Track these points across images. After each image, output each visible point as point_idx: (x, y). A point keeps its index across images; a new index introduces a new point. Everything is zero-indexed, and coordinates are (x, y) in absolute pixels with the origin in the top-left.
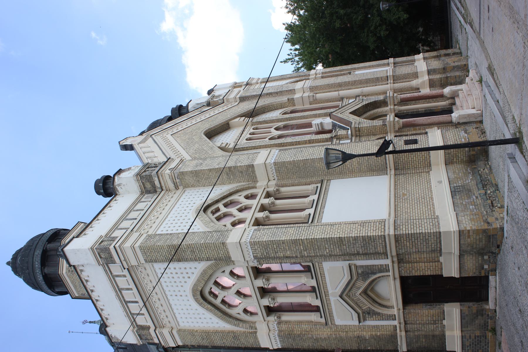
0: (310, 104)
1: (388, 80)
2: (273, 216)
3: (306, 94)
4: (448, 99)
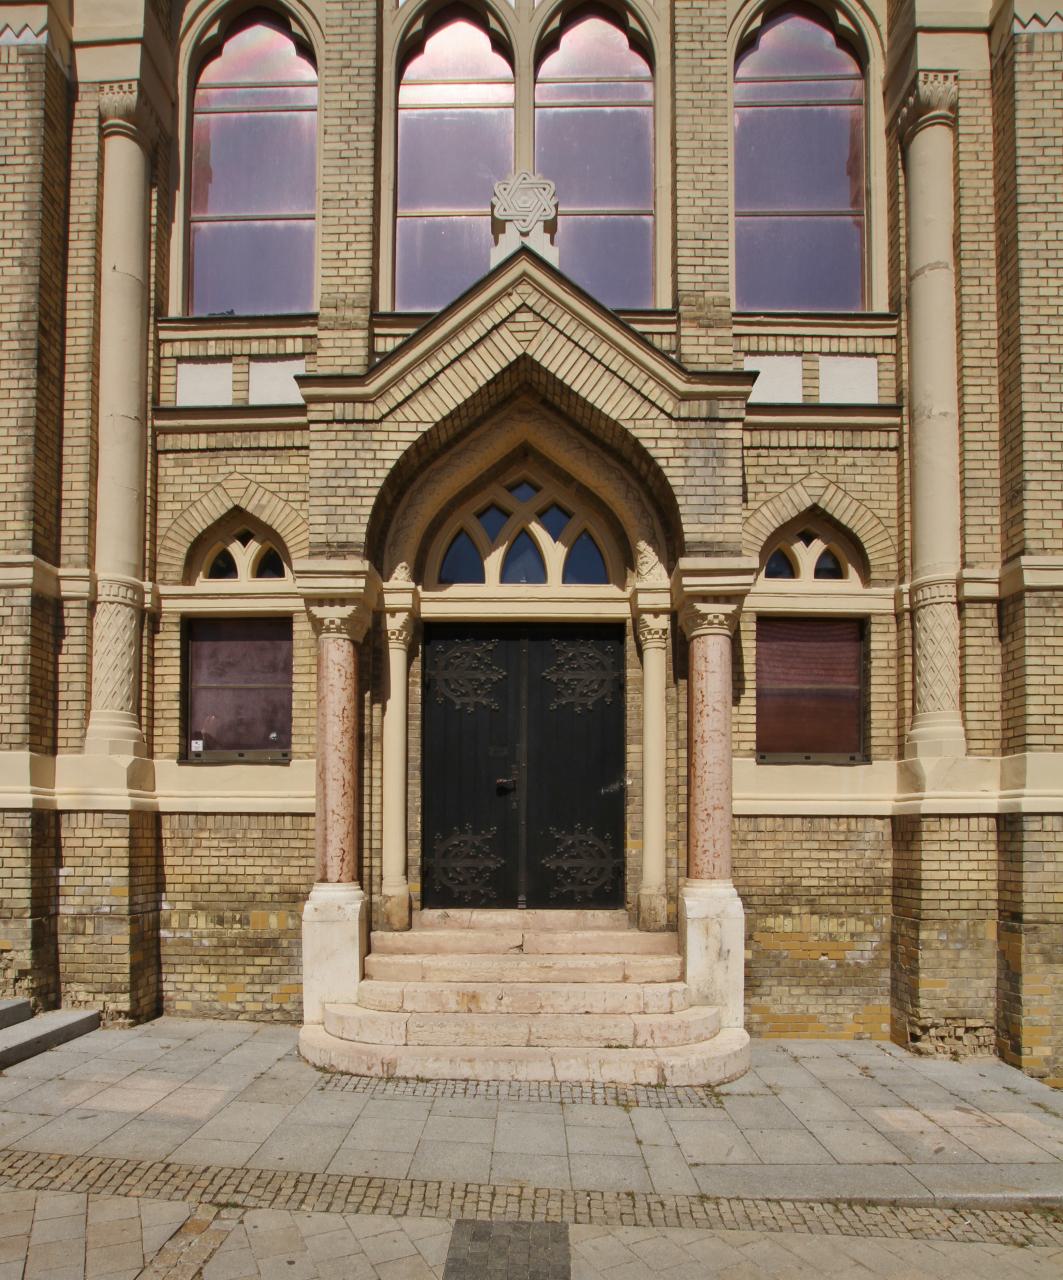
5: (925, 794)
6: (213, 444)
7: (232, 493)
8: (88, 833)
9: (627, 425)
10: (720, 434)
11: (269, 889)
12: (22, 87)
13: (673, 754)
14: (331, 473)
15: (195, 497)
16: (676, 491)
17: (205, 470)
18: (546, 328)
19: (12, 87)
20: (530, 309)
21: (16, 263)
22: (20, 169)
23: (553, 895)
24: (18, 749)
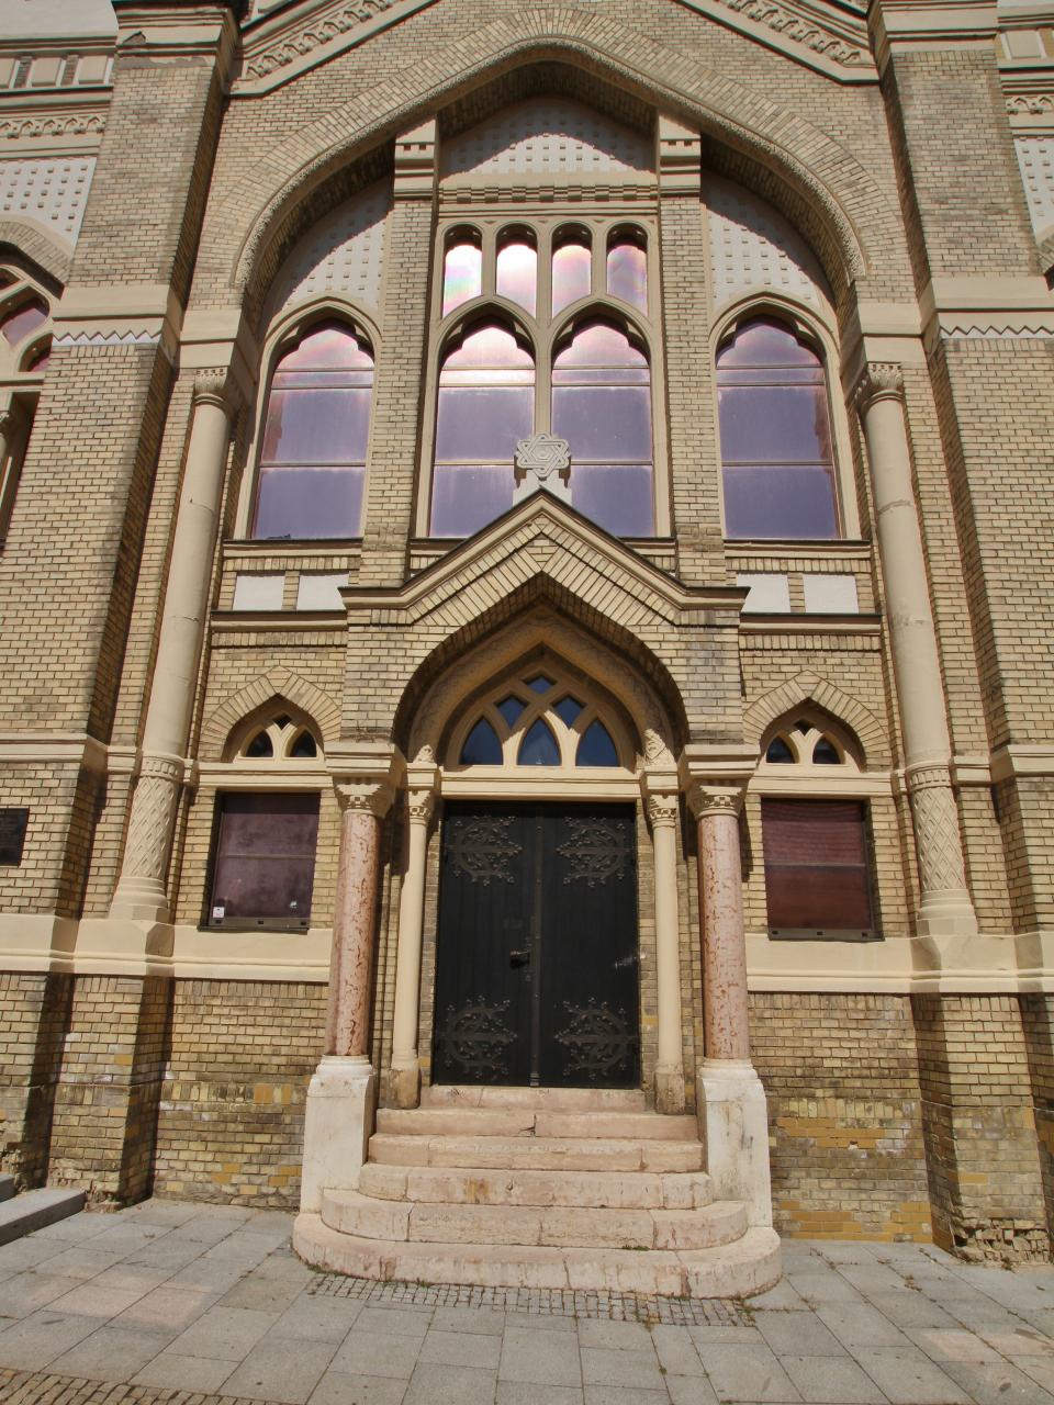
6: (261, 642)
7: (274, 683)
8: (100, 998)
9: (635, 630)
11: (276, 1060)
13: (685, 929)
15: (240, 686)
16: (680, 686)
20: (547, 537)
23: (566, 1072)
24: (44, 912)
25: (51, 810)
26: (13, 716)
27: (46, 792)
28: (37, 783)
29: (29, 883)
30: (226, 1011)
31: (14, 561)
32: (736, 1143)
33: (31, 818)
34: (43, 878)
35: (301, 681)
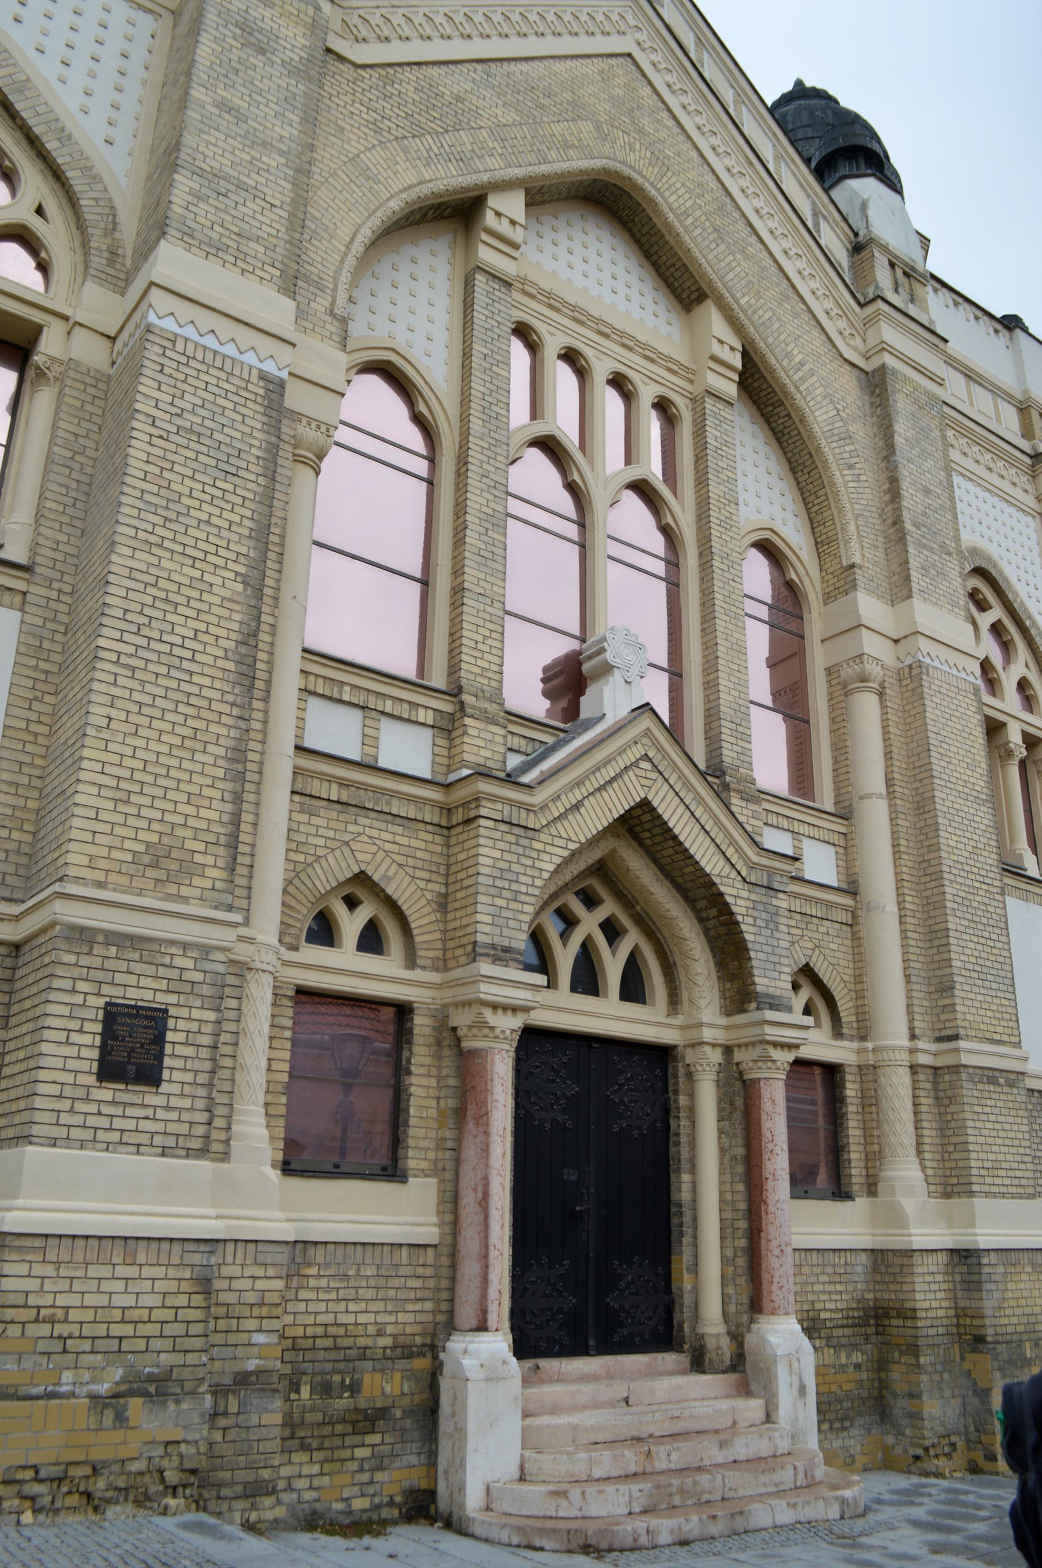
0: (829, 671)
1: (940, 1039)
2: (1014, 771)
3: (872, 645)
4: (737, 1337)
5: (978, 1231)
6: (344, 798)
7: (360, 856)
8: (236, 1271)
9: (717, 880)
10: (775, 902)
11: (383, 1342)
12: (261, 409)
13: (728, 1187)
14: (497, 873)
15: (320, 852)
16: (750, 946)
17: (332, 824)
18: (660, 780)
19: (249, 404)
20: (650, 760)
21: (239, 579)
22: (251, 486)
23: (616, 1338)
24: (196, 1157)
25: (196, 1014)
26: (132, 869)
27: (187, 988)
28: (174, 974)
29: (174, 1115)
30: (323, 1282)
31: (117, 635)
32: (796, 1393)
33: (171, 1023)
34: (192, 1109)
35: (388, 861)
